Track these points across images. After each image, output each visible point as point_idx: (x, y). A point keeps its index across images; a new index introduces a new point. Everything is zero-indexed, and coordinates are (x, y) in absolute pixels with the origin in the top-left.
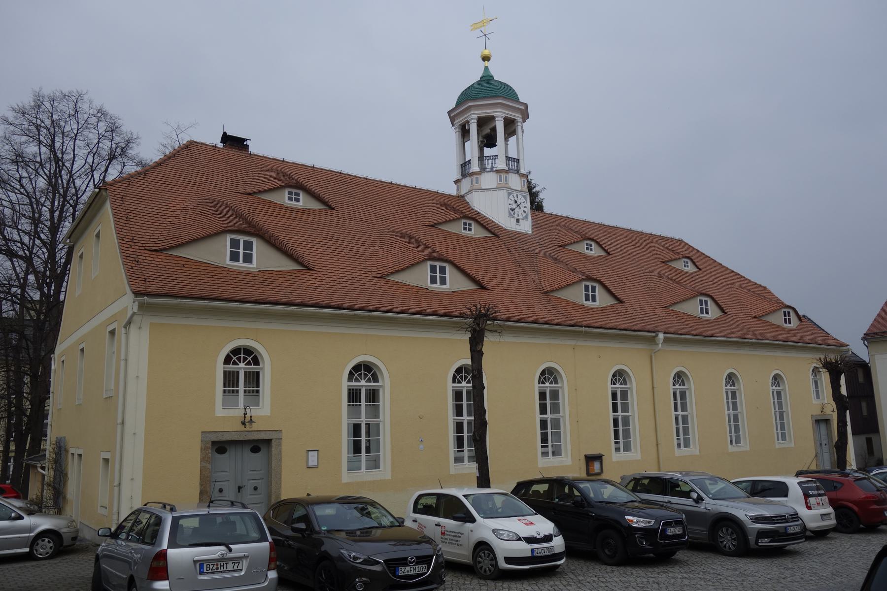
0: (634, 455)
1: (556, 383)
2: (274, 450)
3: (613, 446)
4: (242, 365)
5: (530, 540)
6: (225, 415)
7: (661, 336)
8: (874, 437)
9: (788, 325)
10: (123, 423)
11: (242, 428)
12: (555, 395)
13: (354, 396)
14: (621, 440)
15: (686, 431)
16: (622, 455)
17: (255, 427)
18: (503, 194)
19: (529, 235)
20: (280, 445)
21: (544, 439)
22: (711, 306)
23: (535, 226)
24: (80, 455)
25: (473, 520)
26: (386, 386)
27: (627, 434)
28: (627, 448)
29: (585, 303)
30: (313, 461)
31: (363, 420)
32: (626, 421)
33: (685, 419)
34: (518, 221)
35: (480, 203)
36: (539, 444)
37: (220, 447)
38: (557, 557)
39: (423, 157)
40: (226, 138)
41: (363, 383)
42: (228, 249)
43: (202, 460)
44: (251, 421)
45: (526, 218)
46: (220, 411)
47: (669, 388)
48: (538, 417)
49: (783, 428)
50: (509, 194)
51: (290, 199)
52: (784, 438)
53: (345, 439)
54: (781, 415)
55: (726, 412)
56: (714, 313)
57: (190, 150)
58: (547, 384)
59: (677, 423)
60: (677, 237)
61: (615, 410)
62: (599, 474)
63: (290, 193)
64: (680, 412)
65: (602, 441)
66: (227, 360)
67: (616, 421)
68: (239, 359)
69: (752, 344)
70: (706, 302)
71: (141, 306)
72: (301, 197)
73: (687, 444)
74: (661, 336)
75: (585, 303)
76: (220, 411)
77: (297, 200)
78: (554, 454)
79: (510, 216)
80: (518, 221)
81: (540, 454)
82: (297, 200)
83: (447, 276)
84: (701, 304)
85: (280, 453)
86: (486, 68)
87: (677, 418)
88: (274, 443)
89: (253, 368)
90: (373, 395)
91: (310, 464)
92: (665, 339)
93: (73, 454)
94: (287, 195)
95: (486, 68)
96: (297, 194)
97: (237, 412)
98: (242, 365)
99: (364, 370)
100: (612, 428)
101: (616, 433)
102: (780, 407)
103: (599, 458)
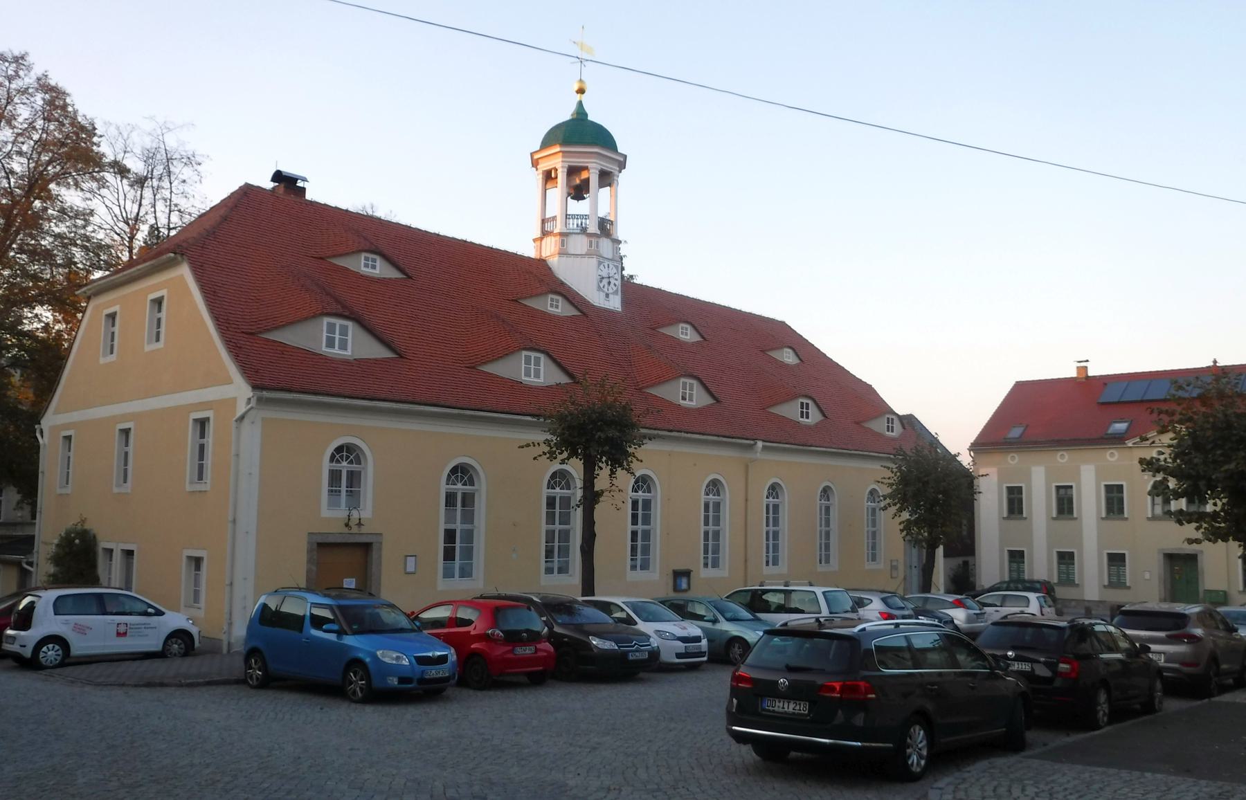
0: (723, 572)
1: (649, 492)
2: (375, 555)
3: (629, 562)
4: (345, 464)
5: (684, 640)
6: (330, 516)
7: (760, 444)
8: (969, 559)
9: (805, 420)
10: (234, 521)
11: (346, 530)
12: (647, 504)
13: (450, 499)
14: (639, 557)
15: (716, 550)
16: (711, 572)
17: (364, 530)
18: (594, 261)
19: (618, 313)
20: (380, 549)
21: (549, 553)
22: (813, 410)
23: (625, 302)
24: (129, 554)
25: (636, 623)
26: (482, 489)
27: (646, 550)
28: (645, 566)
29: (682, 402)
30: (411, 568)
31: (458, 526)
32: (646, 535)
33: (776, 535)
34: (607, 295)
35: (564, 270)
36: (543, 559)
37: (322, 546)
38: (701, 654)
39: (494, 206)
40: (278, 176)
41: (459, 486)
42: (325, 334)
43: (309, 561)
44: (360, 524)
45: (616, 293)
46: (326, 512)
47: (762, 500)
48: (630, 528)
49: (874, 548)
50: (600, 263)
51: (366, 266)
52: (874, 559)
53: (702, 561)
54: (874, 533)
55: (765, 529)
56: (814, 417)
57: (248, 192)
58: (558, 490)
59: (767, 539)
60: (779, 318)
61: (635, 522)
62: (685, 591)
63: (367, 259)
64: (771, 528)
65: (692, 558)
66: (332, 458)
67: (634, 534)
68: (342, 457)
69: (851, 455)
70: (691, 385)
71: (260, 400)
72: (378, 264)
73: (716, 564)
74: (760, 444)
75: (682, 402)
76: (326, 512)
77: (374, 267)
78: (560, 571)
79: (599, 289)
80: (607, 295)
81: (543, 570)
82: (374, 267)
83: (542, 368)
84: (685, 388)
85: (380, 557)
86: (580, 103)
87: (767, 533)
88: (375, 547)
89: (354, 467)
90: (468, 500)
91: (409, 570)
92: (764, 448)
93: (110, 552)
94: (363, 261)
95: (580, 103)
96: (374, 260)
97: (341, 513)
98: (345, 464)
99: (345, 452)
100: (629, 543)
101: (634, 549)
102: (874, 525)
103: (687, 574)
